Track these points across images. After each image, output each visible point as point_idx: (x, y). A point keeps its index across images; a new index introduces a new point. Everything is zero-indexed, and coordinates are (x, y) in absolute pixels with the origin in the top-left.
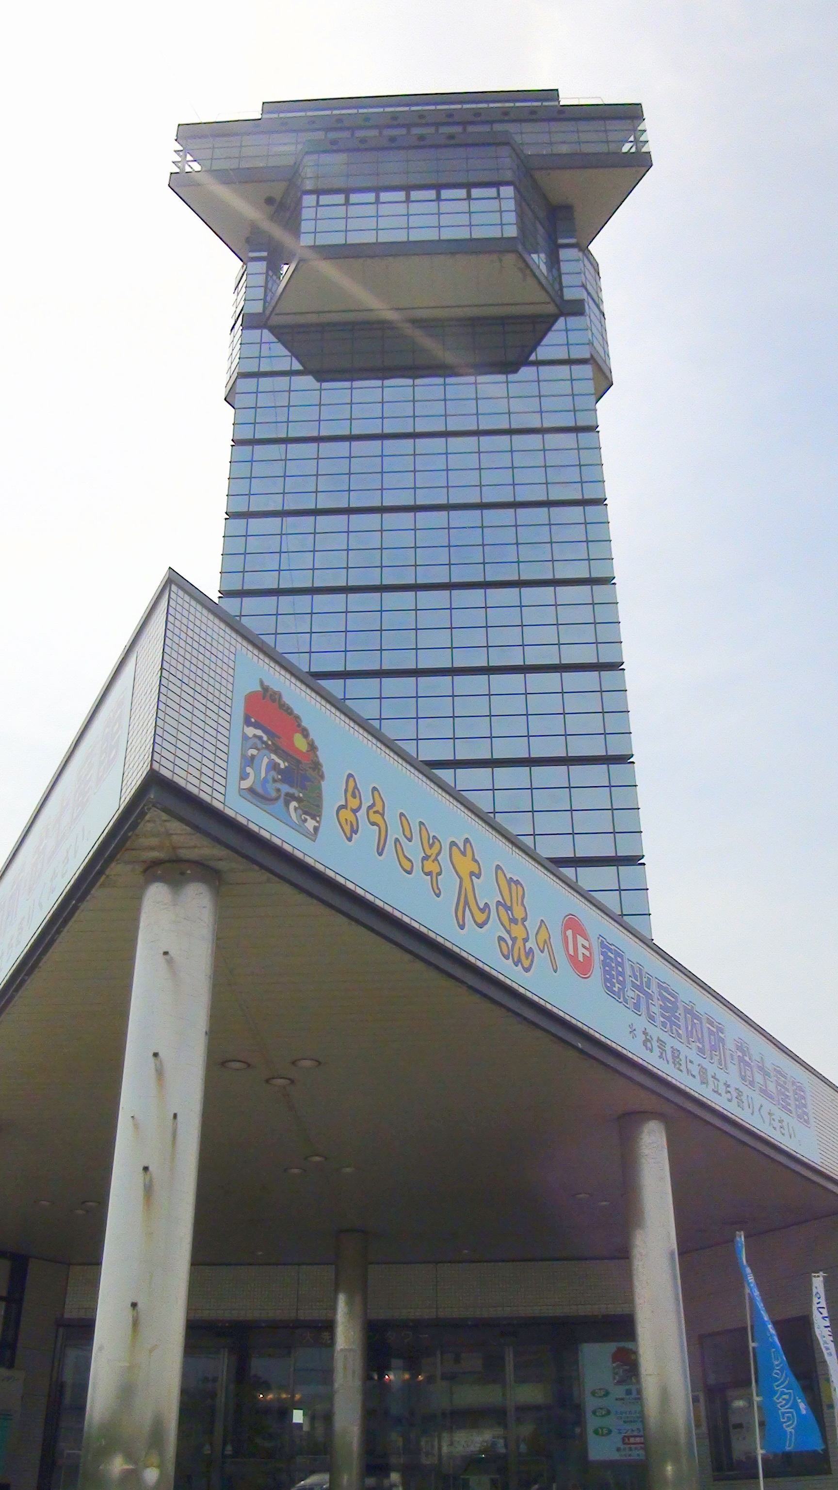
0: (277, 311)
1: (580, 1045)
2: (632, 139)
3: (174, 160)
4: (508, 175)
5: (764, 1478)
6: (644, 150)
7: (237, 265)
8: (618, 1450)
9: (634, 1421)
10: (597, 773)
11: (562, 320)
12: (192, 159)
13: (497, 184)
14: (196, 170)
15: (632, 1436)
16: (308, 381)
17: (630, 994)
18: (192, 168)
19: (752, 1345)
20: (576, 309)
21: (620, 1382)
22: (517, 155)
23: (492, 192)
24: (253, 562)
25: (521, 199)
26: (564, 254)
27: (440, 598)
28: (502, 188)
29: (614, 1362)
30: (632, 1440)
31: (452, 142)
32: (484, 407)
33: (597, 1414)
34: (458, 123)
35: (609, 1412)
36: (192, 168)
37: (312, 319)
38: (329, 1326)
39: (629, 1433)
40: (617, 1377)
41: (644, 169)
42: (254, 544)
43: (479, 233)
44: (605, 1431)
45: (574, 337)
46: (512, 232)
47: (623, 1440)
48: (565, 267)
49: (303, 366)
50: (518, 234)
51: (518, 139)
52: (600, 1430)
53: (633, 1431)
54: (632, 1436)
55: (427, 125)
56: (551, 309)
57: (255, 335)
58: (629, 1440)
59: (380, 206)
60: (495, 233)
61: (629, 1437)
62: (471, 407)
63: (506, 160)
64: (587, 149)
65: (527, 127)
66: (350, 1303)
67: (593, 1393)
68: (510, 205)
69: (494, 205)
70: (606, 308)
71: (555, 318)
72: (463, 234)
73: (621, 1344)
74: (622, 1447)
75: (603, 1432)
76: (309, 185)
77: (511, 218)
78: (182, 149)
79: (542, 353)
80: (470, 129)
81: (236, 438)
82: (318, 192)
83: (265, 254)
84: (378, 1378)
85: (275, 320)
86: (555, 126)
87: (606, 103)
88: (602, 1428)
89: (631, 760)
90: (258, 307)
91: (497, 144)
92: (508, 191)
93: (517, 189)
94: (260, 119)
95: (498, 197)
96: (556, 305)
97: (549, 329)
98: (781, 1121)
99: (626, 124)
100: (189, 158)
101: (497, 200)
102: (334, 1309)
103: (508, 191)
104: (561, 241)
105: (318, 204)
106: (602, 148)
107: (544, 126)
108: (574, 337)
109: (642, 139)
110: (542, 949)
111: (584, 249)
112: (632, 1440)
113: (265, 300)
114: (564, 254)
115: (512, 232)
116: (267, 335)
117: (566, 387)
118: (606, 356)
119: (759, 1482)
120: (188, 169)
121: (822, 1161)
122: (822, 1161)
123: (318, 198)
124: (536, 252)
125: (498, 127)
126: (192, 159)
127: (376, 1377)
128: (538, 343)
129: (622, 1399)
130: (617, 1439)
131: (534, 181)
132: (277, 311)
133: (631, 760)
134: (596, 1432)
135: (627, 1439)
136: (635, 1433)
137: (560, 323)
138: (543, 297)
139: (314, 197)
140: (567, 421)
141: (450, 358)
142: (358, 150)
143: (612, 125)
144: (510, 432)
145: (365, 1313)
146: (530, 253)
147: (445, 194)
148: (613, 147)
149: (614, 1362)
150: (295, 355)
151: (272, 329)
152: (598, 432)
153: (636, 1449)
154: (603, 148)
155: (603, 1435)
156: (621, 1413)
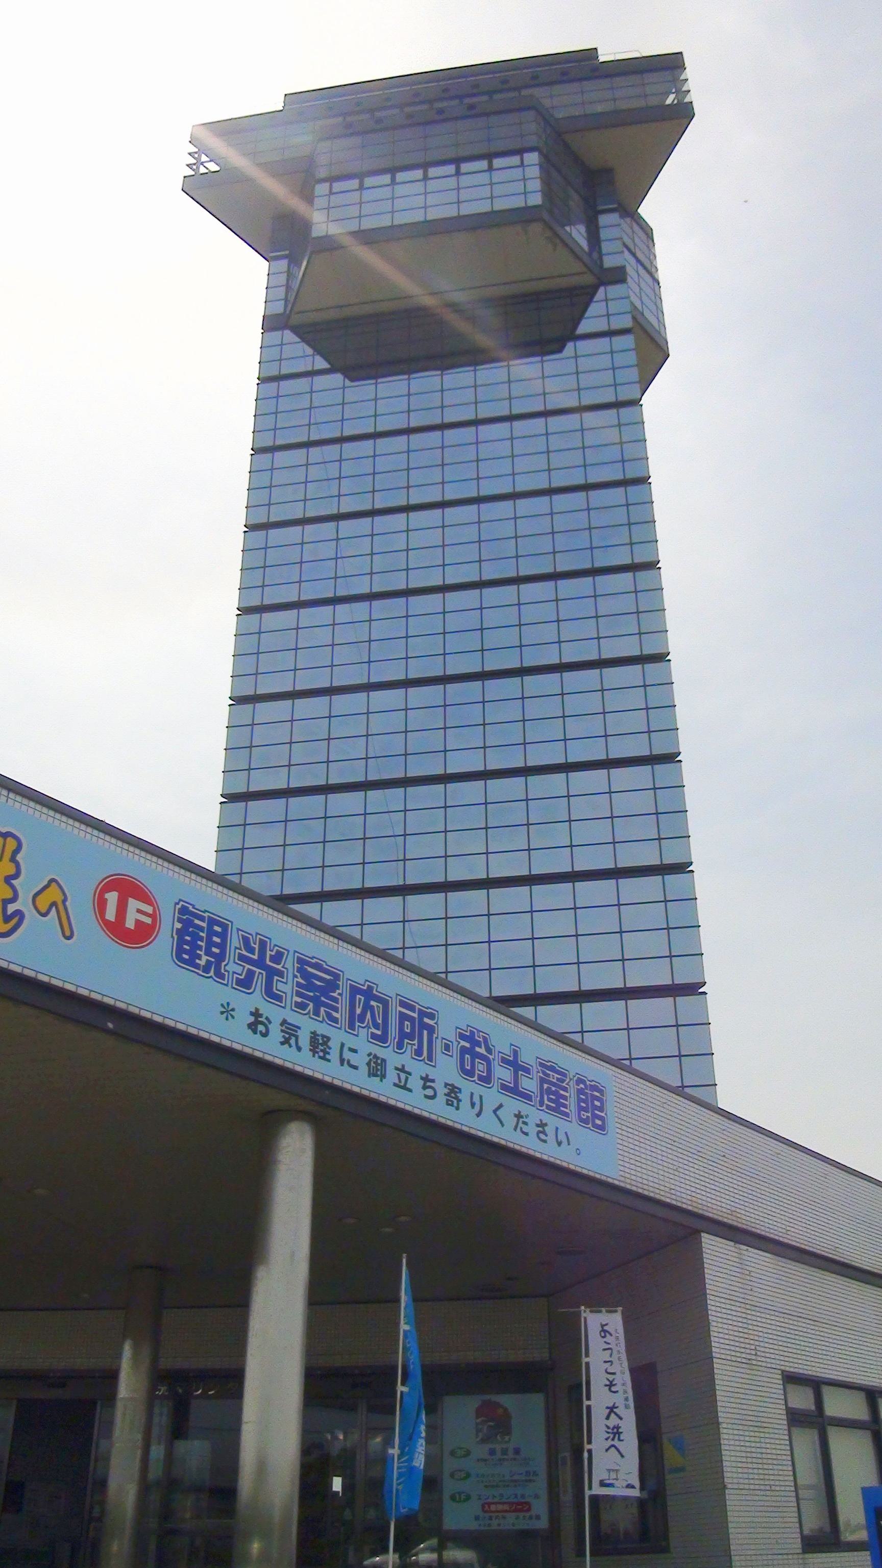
0: (296, 309)
1: (110, 1025)
2: (674, 90)
3: (188, 163)
4: (532, 141)
5: (591, 1556)
6: (686, 100)
7: (263, 266)
8: (477, 1518)
9: (497, 1486)
10: (640, 775)
11: (601, 290)
12: (208, 159)
13: (520, 152)
14: (213, 170)
15: (493, 1503)
16: (337, 379)
17: (232, 967)
18: (207, 169)
19: (400, 1388)
20: (618, 276)
21: (484, 1441)
22: (545, 119)
23: (515, 160)
24: (272, 575)
25: (548, 166)
26: (604, 220)
27: (470, 597)
28: (526, 155)
29: (477, 1417)
30: (493, 1508)
31: (473, 112)
32: (517, 390)
33: (456, 1477)
34: (483, 94)
35: (468, 1475)
36: (207, 169)
37: (332, 315)
38: (112, 1376)
39: (490, 1500)
40: (480, 1435)
41: (686, 121)
42: (273, 556)
43: (501, 205)
44: (463, 1497)
45: (614, 307)
46: (536, 200)
47: (483, 1506)
48: (604, 234)
49: (329, 363)
50: (543, 202)
51: (547, 103)
52: (458, 1497)
53: (494, 1497)
54: (493, 1503)
55: (451, 98)
56: (588, 279)
57: (276, 336)
58: (489, 1507)
59: (396, 187)
60: (518, 202)
61: (489, 1504)
62: (503, 391)
63: (530, 125)
64: (623, 105)
65: (557, 89)
66: (136, 1348)
67: (453, 1453)
68: (534, 172)
69: (517, 173)
70: (662, 275)
71: (595, 288)
72: (484, 207)
73: (487, 1397)
74: (481, 1514)
75: (459, 1498)
76: (322, 173)
77: (535, 185)
78: (196, 150)
79: (585, 327)
80: (497, 97)
81: (256, 446)
82: (331, 180)
83: (287, 252)
84: (344, 1437)
85: (296, 320)
86: (588, 85)
87: (644, 55)
88: (460, 1493)
89: (678, 759)
90: (279, 308)
91: (520, 110)
92: (532, 158)
93: (541, 153)
94: (281, 111)
95: (522, 165)
96: (595, 275)
97: (590, 300)
98: (542, 1125)
99: (667, 75)
100: (204, 158)
101: (521, 169)
102: (119, 1356)
103: (532, 158)
104: (600, 208)
105: (331, 193)
106: (641, 103)
107: (575, 86)
108: (614, 307)
109: (684, 89)
110: (54, 909)
111: (630, 213)
112: (493, 1508)
113: (286, 300)
114: (604, 220)
115: (536, 200)
116: (289, 336)
117: (605, 361)
118: (661, 325)
119: (585, 1562)
120: (202, 170)
121: (622, 1173)
122: (622, 1173)
123: (331, 185)
124: (570, 224)
125: (524, 92)
126: (208, 159)
127: (341, 1437)
128: (581, 317)
129: (485, 1460)
130: (474, 1507)
131: (566, 146)
132: (296, 309)
133: (678, 759)
134: (453, 1498)
135: (486, 1506)
136: (496, 1500)
137: (601, 293)
138: (577, 267)
139: (328, 184)
140: (608, 396)
141: (483, 340)
142: (374, 131)
143: (650, 78)
144: (545, 414)
145: (155, 1361)
146: (563, 226)
147: (465, 167)
148: (653, 101)
149: (477, 1417)
150: (318, 351)
151: (296, 330)
152: (641, 405)
153: (497, 1517)
154: (641, 103)
155: (460, 1501)
156: (483, 1476)
